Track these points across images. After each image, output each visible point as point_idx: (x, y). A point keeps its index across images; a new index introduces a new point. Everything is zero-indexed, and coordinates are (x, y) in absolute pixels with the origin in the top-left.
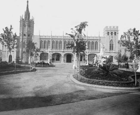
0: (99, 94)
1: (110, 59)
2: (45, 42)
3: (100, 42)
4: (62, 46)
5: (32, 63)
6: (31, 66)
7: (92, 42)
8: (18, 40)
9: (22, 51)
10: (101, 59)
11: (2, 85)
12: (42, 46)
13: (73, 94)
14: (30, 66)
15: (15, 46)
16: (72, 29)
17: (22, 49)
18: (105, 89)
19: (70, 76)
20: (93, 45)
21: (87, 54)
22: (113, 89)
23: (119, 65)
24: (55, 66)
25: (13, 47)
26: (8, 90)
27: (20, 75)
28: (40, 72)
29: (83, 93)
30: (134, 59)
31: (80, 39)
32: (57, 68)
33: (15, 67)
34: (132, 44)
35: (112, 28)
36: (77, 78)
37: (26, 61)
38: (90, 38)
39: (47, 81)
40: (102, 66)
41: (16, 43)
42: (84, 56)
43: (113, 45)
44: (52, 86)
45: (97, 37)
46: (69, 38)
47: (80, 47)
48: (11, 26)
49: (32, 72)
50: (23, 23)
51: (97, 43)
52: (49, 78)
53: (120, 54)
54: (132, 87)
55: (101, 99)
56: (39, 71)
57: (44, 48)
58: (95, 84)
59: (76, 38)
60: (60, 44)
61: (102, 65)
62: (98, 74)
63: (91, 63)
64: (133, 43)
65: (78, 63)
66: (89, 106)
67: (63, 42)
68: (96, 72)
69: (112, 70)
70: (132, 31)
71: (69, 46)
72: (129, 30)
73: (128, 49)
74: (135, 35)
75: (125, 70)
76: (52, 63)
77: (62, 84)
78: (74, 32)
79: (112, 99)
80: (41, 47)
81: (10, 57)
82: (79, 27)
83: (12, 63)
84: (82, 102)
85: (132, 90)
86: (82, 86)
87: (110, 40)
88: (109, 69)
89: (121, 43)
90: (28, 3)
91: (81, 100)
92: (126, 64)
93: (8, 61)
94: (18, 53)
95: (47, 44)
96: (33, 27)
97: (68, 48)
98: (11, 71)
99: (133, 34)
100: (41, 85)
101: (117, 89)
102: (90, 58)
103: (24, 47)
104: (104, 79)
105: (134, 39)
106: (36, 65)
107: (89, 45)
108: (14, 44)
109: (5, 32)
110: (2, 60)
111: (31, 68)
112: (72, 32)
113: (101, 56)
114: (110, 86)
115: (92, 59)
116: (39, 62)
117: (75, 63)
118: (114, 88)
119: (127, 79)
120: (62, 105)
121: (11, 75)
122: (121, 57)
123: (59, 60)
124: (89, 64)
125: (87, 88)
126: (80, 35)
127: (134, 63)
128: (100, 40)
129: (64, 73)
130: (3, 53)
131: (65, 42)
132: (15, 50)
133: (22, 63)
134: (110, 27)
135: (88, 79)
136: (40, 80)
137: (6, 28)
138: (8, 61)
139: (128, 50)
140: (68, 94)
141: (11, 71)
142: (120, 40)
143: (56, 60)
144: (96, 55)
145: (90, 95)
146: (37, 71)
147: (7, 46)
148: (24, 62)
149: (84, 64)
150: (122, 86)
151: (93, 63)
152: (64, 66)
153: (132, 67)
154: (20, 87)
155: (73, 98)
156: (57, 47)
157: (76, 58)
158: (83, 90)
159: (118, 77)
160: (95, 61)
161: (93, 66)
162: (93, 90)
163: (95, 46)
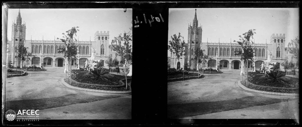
0: (90, 98)
1: (101, 64)
2: (37, 46)
3: (267, 49)
4: (54, 51)
5: (201, 70)
6: (199, 73)
7: (227, 49)
8: (186, 47)
9: (14, 55)
10: (269, 66)
11: (171, 91)
12: (33, 51)
13: (241, 100)
14: (198, 73)
15: (183, 53)
16: (63, 34)
17: (190, 56)
18: (96, 93)
19: (237, 82)
20: (84, 50)
21: (79, 59)
22: (104, 93)
23: (110, 69)
24: (46, 70)
25: (181, 54)
26: (176, 96)
27: (188, 81)
28: (32, 76)
29: (251, 99)
30: (125, 63)
31: (71, 44)
32: (49, 72)
33: (183, 74)
34: (123, 48)
35: (103, 32)
36: (68, 82)
37: (194, 68)
38: (210, 44)
39: (215, 87)
40: (93, 71)
41: (185, 51)
42: (76, 60)
43: (104, 49)
44: (43, 89)
45: (88, 42)
46: (60, 43)
47: (71, 51)
48: (180, 34)
49: (200, 78)
50: (191, 31)
51: (88, 47)
52: (41, 81)
53: (111, 58)
54: (123, 91)
55: (92, 102)
56: (30, 75)
57: (36, 52)
58: (86, 87)
59: (67, 43)
60: (51, 48)
61: (93, 70)
62: (266, 81)
63: (82, 67)
64: (124, 48)
65: (69, 68)
66: (80, 109)
67: (54, 47)
68: (87, 76)
69: (103, 74)
70: (122, 36)
71: (61, 50)
72: (120, 35)
73: (119, 53)
74: (125, 40)
75: (116, 74)
76: (44, 67)
77: (54, 88)
78: (66, 37)
79: (103, 103)
80: (32, 51)
81: (179, 64)
82: (70, 32)
83: (181, 70)
84: (73, 105)
85: (122, 93)
86: (250, 92)
87: (101, 44)
88: (100, 73)
89: (112, 48)
90: (196, 11)
91: (72, 103)
92: (117, 69)
93: (176, 68)
94: (186, 60)
95: (39, 48)
96: (201, 35)
97: (59, 52)
98: (180, 78)
99: (123, 39)
100: (32, 89)
101: (107, 93)
102: (81, 63)
103: (192, 54)
104: (95, 83)
105: (125, 44)
106: (28, 69)
107: (80, 50)
108: (182, 52)
109: (173, 39)
110: (170, 67)
111: (199, 75)
112: (63, 37)
113: (92, 60)
114: (278, 92)
115: (83, 64)
116: (31, 66)
117: (66, 67)
118: (105, 91)
119: (118, 83)
120: (54, 108)
121: (179, 82)
122: (112, 61)
123: (50, 64)
124: (80, 68)
125: (79, 91)
126: (71, 39)
127: (125, 67)
128: (91, 44)
129: (55, 77)
130: (171, 60)
131: (56, 47)
132: (183, 57)
133: (14, 68)
134: (277, 35)
135: (79, 83)
136: (31, 84)
137: (175, 35)
138: (176, 68)
139: (119, 54)
140: (59, 97)
141: (180, 78)
142: (111, 44)
143: (48, 64)
144: (87, 59)
145: (81, 99)
146: (28, 75)
147: (175, 53)
148: (192, 69)
149: (75, 68)
150: (113, 90)
151: (85, 67)
152: (55, 70)
153: (123, 71)
154: (189, 94)
155: (64, 101)
156: (49, 51)
157: (67, 62)
158: (74, 93)
159: (109, 81)
160: (86, 65)
161: (84, 70)
162: (261, 97)
163: (86, 50)
